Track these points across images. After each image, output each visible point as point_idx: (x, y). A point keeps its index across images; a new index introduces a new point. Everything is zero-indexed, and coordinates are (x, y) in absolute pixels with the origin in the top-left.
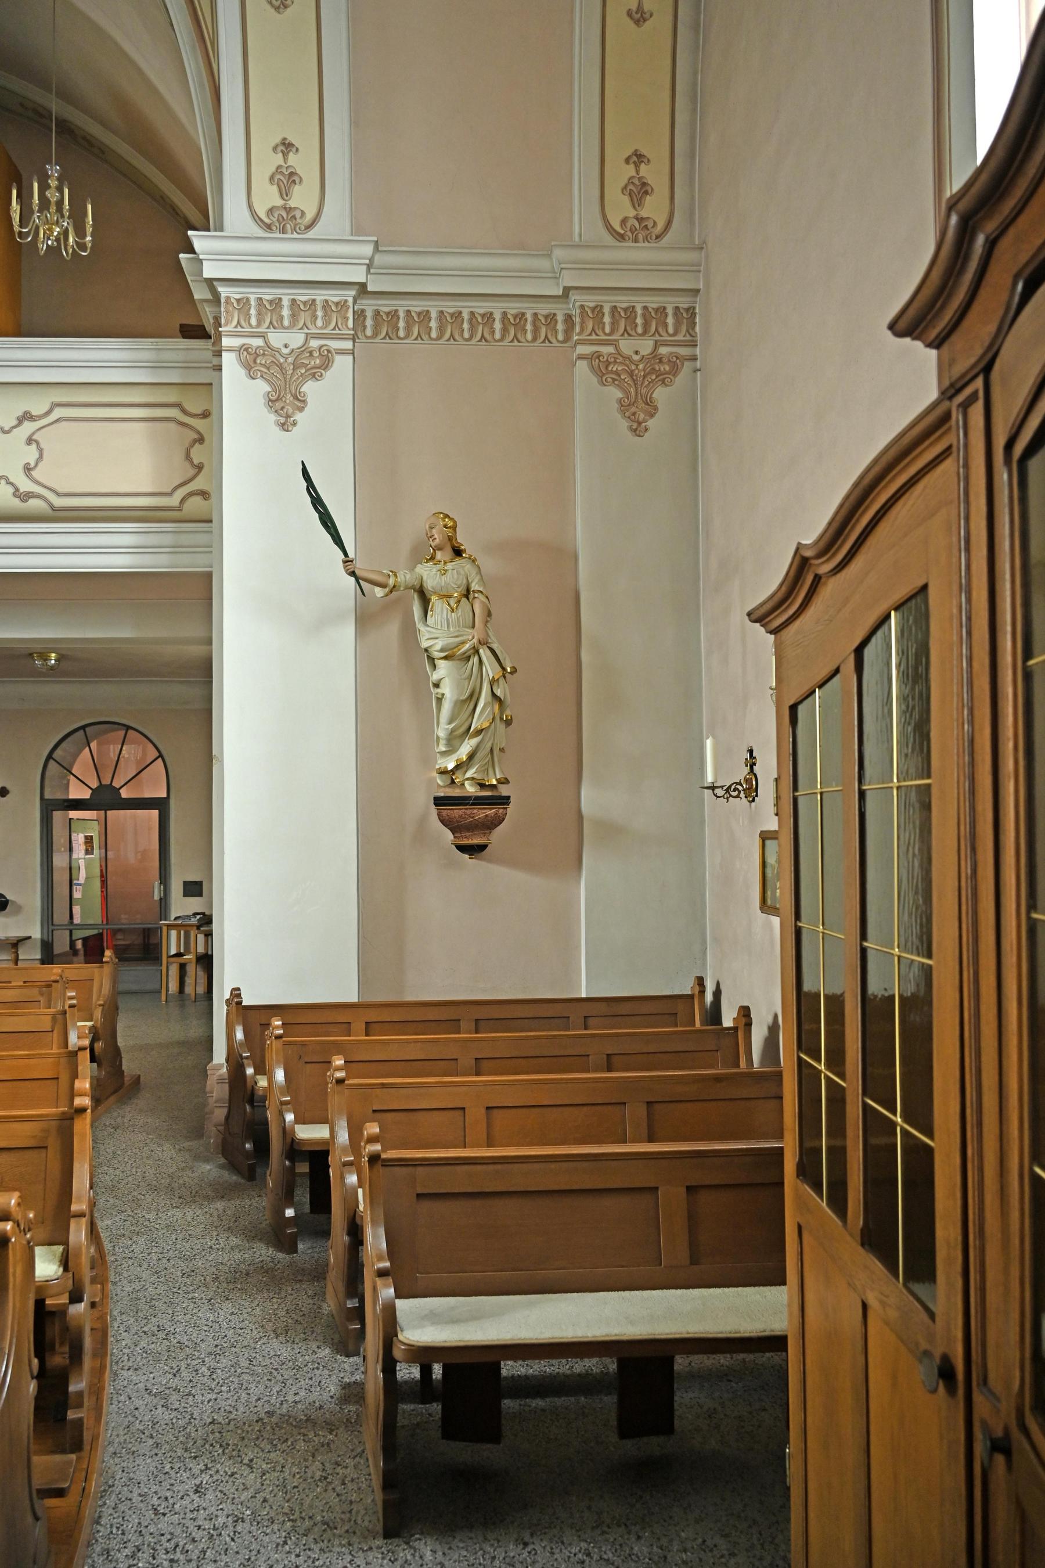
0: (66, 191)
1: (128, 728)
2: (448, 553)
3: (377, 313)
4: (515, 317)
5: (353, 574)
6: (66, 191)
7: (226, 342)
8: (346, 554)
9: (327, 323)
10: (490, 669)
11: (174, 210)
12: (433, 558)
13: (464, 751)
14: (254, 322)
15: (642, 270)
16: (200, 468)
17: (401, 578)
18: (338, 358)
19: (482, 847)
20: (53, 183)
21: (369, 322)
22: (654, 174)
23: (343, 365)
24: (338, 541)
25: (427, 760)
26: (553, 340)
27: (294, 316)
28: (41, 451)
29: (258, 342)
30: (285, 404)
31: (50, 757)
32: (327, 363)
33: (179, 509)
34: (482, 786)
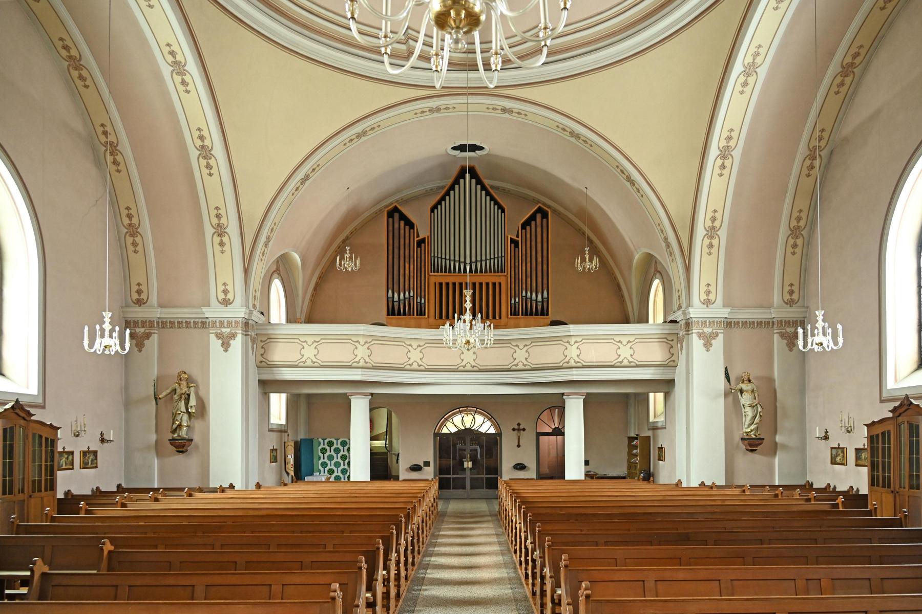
10: (760, 409)
13: (752, 427)
15: (792, 313)
22: (796, 288)
23: (721, 336)
30: (708, 345)
32: (717, 336)
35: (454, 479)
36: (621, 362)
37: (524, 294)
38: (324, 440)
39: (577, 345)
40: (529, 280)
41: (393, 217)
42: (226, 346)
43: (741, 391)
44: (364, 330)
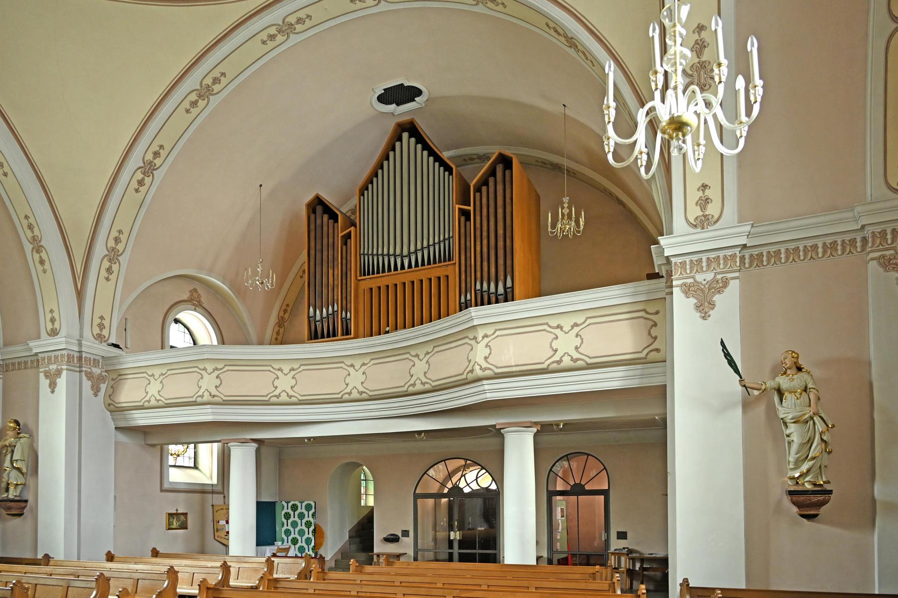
1: (588, 455)
2: (794, 370)
3: (751, 256)
4: (831, 244)
5: (744, 386)
7: (674, 283)
8: (741, 377)
9: (725, 265)
10: (820, 426)
12: (785, 373)
13: (805, 467)
14: (688, 271)
16: (655, 338)
17: (768, 385)
18: (732, 282)
19: (816, 516)
20: (566, 205)
21: (747, 261)
23: (734, 285)
24: (737, 371)
25: (781, 472)
26: (854, 252)
27: (708, 265)
28: (582, 339)
29: (691, 280)
30: (704, 307)
31: (551, 470)
32: (725, 283)
33: (645, 358)
34: (815, 485)
35: (479, 554)
36: (559, 362)
37: (478, 287)
38: (288, 503)
39: (486, 340)
40: (485, 264)
41: (314, 212)
42: (53, 386)
43: (780, 393)
44: (484, 392)
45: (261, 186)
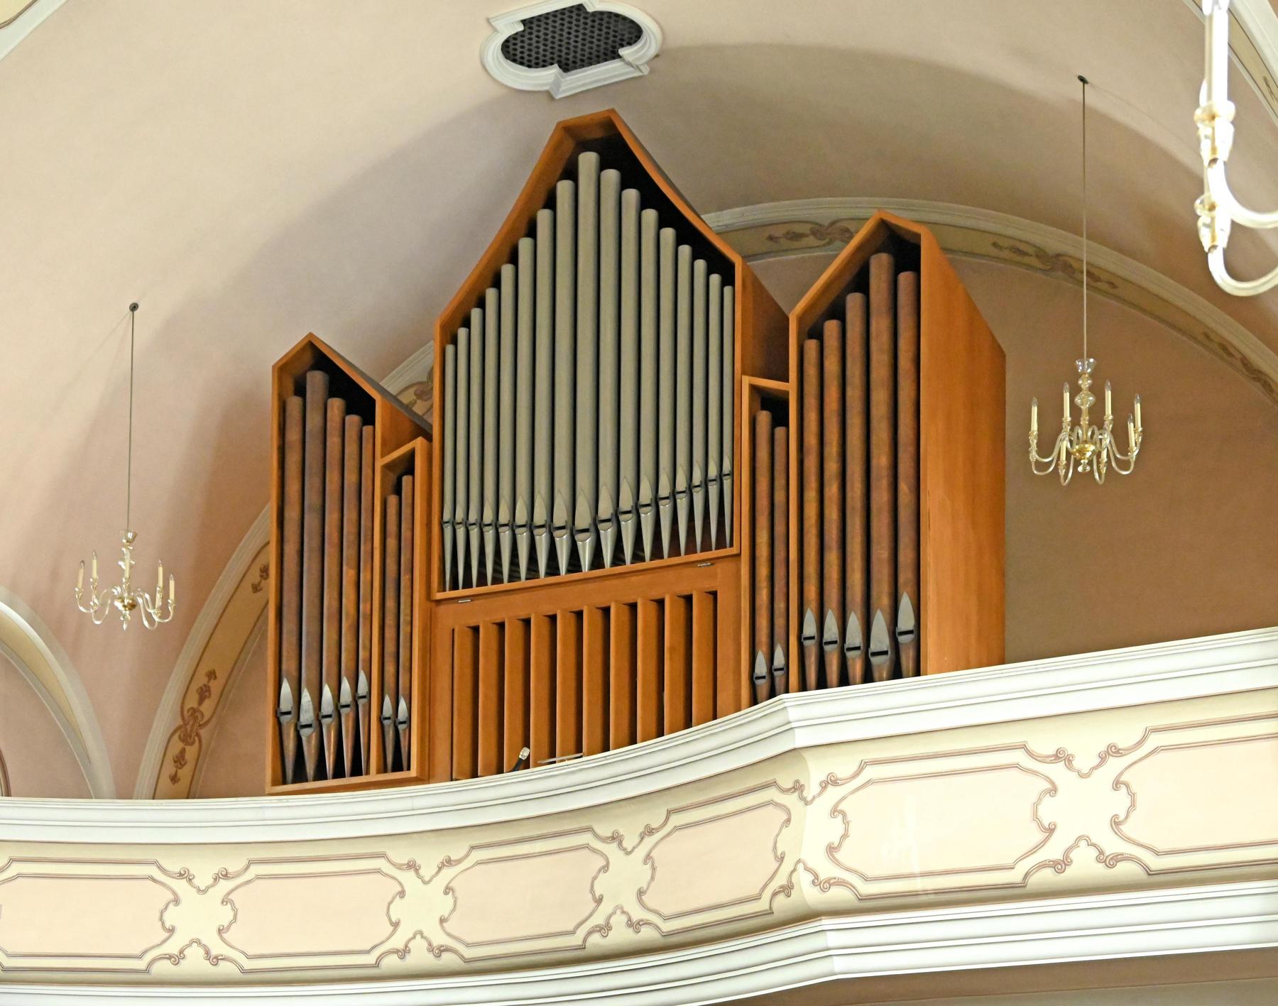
0: (1108, 394)
6: (1108, 394)
11: (1224, 348)
20: (1085, 383)
28: (1132, 796)
36: (1061, 865)
37: (810, 628)
40: (832, 557)
41: (300, 390)
45: (134, 307)
